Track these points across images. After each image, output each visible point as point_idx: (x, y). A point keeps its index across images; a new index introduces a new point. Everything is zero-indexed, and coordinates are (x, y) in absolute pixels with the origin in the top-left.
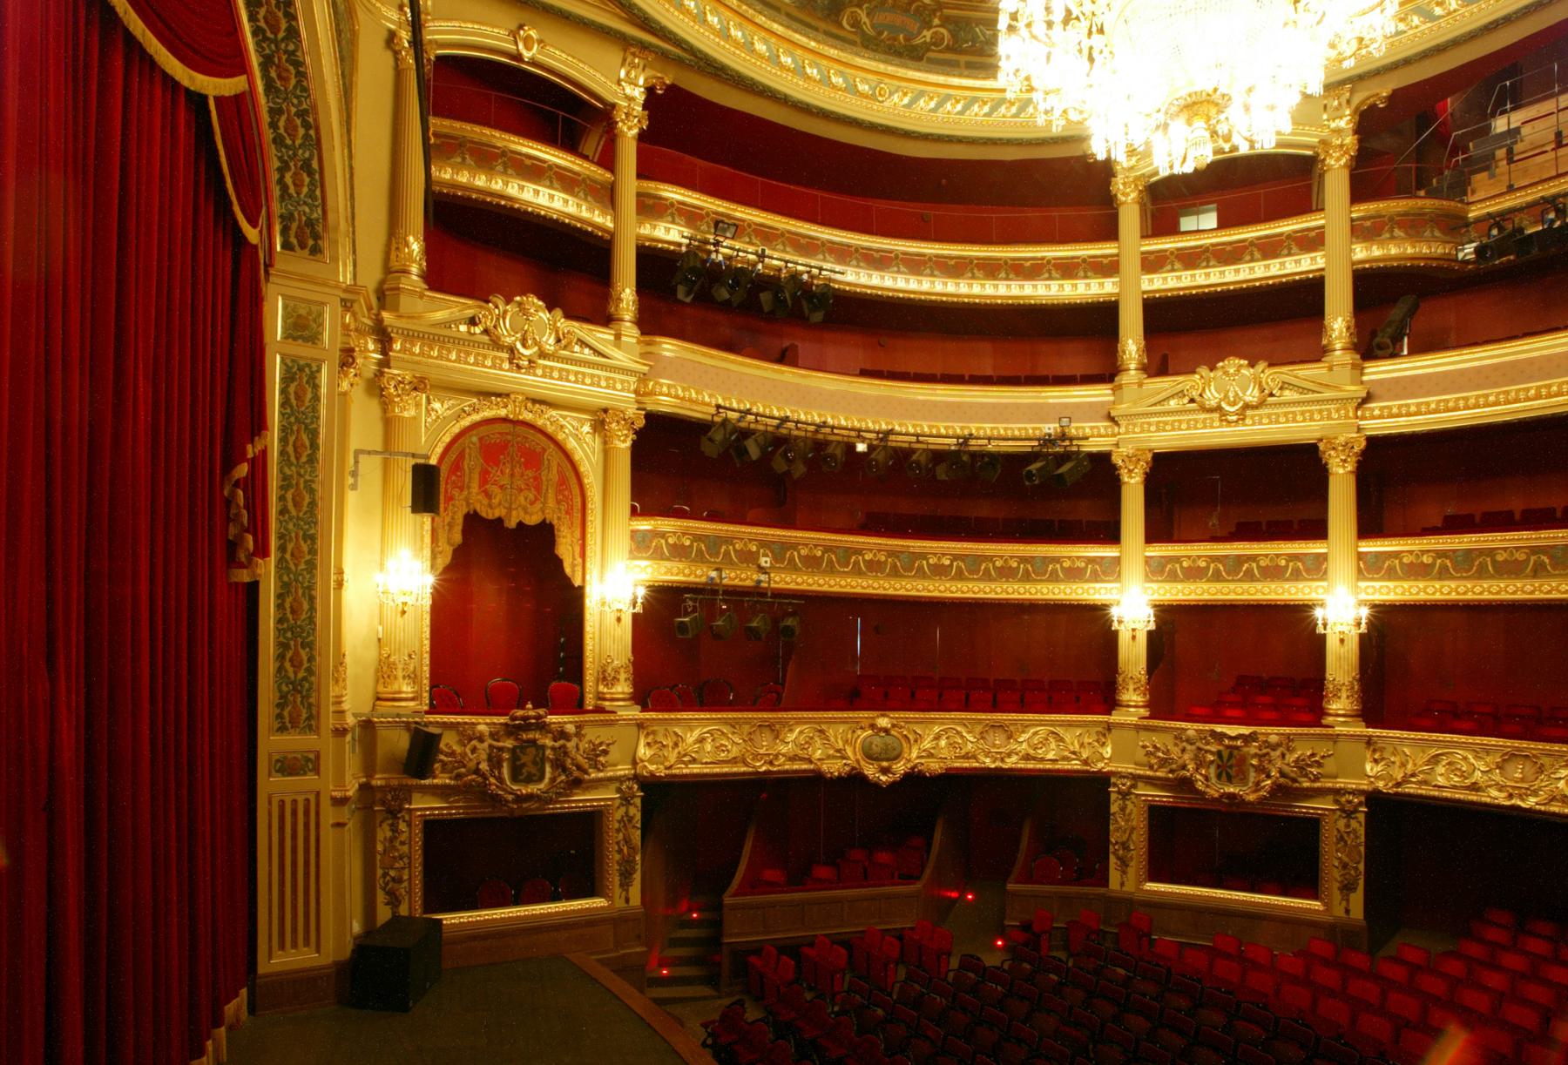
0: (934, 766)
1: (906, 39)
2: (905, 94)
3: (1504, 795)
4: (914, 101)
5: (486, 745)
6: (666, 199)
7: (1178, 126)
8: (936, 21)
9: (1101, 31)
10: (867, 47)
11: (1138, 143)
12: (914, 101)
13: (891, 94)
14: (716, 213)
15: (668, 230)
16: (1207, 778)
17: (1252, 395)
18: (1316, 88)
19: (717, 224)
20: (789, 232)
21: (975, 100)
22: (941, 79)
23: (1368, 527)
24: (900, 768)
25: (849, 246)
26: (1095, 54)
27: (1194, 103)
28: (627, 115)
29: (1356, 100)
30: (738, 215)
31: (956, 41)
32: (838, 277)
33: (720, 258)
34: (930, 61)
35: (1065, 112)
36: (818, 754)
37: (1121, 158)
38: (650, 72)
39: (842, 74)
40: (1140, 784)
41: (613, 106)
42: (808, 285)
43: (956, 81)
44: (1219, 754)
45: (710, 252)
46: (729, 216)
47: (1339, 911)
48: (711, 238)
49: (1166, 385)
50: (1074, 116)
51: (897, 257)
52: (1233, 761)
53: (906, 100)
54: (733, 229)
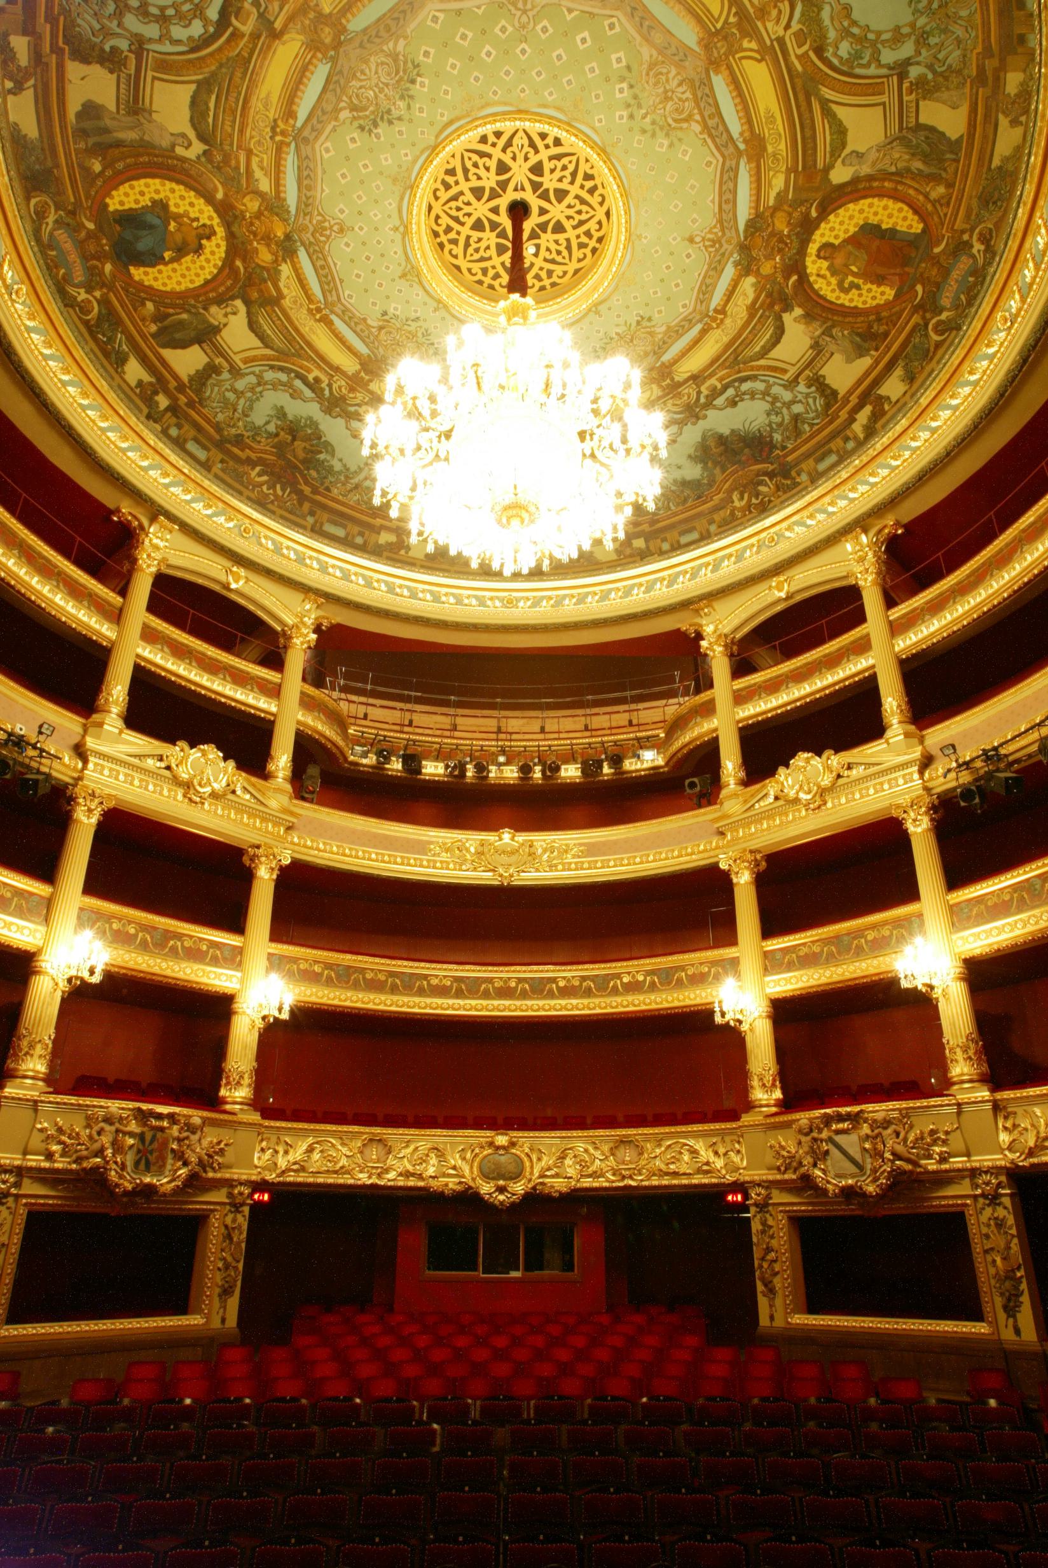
0: (559, 1185)
3: (366, 1175)
5: (113, 1128)
8: (98, 294)
16: (123, 1167)
17: (826, 781)
23: (771, 927)
24: (519, 1188)
31: (98, 325)
36: (431, 1171)
40: (26, 1182)
44: (141, 1137)
47: (216, 1324)
49: (140, 742)
52: (155, 1145)
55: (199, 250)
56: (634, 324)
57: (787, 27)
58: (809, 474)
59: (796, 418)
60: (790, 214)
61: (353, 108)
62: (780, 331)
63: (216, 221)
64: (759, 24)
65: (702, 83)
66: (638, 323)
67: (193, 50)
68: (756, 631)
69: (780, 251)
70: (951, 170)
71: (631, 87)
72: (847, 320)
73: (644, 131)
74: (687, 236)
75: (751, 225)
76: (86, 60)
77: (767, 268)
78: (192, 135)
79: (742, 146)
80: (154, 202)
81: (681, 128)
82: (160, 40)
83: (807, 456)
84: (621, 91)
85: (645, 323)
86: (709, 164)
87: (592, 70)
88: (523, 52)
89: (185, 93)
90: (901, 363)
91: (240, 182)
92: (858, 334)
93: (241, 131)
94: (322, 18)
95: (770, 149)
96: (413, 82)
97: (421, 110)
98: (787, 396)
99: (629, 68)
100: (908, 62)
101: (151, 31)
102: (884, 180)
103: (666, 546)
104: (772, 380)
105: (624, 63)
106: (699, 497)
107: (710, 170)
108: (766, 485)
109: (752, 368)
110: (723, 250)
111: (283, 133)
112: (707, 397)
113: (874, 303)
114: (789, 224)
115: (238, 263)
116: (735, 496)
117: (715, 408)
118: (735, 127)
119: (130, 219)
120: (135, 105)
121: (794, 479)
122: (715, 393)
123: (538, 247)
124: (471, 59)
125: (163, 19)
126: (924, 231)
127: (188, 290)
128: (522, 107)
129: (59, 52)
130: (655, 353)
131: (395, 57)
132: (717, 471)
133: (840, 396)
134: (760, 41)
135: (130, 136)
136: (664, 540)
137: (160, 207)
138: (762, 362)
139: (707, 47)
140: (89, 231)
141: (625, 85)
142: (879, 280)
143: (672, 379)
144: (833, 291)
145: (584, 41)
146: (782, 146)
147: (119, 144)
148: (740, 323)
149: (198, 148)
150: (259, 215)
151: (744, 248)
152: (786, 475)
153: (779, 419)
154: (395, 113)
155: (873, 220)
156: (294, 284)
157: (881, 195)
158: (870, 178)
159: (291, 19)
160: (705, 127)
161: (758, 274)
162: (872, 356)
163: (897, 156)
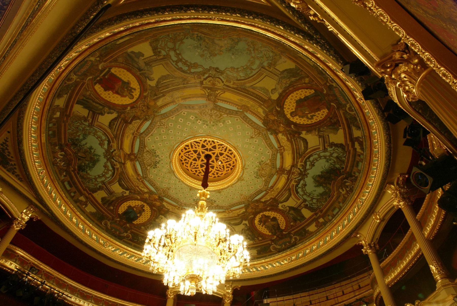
1: (119, 233)
2: (113, 248)
4: (115, 250)
6: (17, 253)
7: (187, 282)
9: (172, 251)
10: (107, 231)
11: (177, 283)
12: (115, 250)
13: (109, 246)
14: (34, 264)
15: (11, 264)
18: (223, 282)
19: (32, 267)
20: (57, 278)
21: (133, 256)
22: (126, 247)
25: (77, 288)
26: (170, 256)
27: (193, 277)
28: (19, 223)
29: (233, 286)
30: (41, 266)
32: (68, 298)
33: (27, 280)
34: (124, 241)
35: (158, 268)
37: (170, 286)
38: (34, 214)
39: (96, 236)
41: (15, 219)
42: (56, 298)
43: (130, 249)
45: (24, 276)
46: (38, 266)
48: (27, 272)
50: (160, 271)
51: (92, 297)
53: (113, 249)
54: (37, 271)
55: (144, 210)
56: (259, 165)
57: (223, 82)
58: (358, 172)
59: (337, 157)
60: (272, 114)
61: (149, 166)
62: (305, 141)
63: (143, 203)
64: (216, 87)
65: (216, 107)
66: (260, 164)
67: (112, 177)
68: (385, 230)
69: (280, 123)
70: (303, 73)
71: (201, 120)
72: (322, 124)
73: (213, 126)
74: (250, 137)
75: (264, 123)
76: (96, 192)
77: (281, 129)
78: (124, 191)
79: (241, 110)
80: (128, 207)
81: (222, 118)
82: (106, 179)
83: (352, 166)
84: (199, 122)
85: (262, 163)
86: (237, 120)
87: (189, 124)
88: (171, 132)
89: (117, 185)
90: (351, 125)
91: (140, 193)
92: (329, 126)
93: (133, 184)
94: (129, 155)
95: (249, 105)
96: (155, 153)
97: (162, 156)
98: (327, 154)
99: (196, 117)
100: (261, 64)
101: (103, 179)
102: (288, 89)
103: (330, 218)
104: (318, 153)
105: (194, 117)
106: (329, 197)
107: (239, 120)
108: (348, 182)
109: (308, 154)
110: (264, 134)
111: (140, 179)
112: (302, 168)
113: (324, 115)
114: (275, 116)
115: (154, 208)
116: (341, 191)
117: (308, 169)
118: (235, 108)
119: (125, 213)
120: (111, 193)
121: (354, 176)
122: (304, 166)
123: (220, 161)
124: (162, 141)
125: (103, 176)
126: (315, 91)
127: (148, 220)
128: (181, 141)
129: (90, 194)
130: (274, 168)
131: (148, 151)
132: (328, 186)
133: (344, 144)
134: (220, 89)
135: (114, 198)
136: (329, 216)
137: (129, 207)
138: (309, 150)
139: (209, 100)
140: (119, 221)
141: (199, 121)
142: (318, 110)
143: (286, 170)
144: (308, 121)
145: (181, 120)
146: (251, 103)
147: (113, 201)
148: (290, 146)
149: (128, 192)
150: (150, 197)
151: (269, 129)
152: (352, 176)
153: (332, 161)
154: (158, 161)
155: (298, 98)
156: (169, 205)
157: (292, 92)
158: (284, 91)
159: (124, 159)
160: (227, 114)
161: (280, 132)
162: (341, 129)
163: (285, 82)
